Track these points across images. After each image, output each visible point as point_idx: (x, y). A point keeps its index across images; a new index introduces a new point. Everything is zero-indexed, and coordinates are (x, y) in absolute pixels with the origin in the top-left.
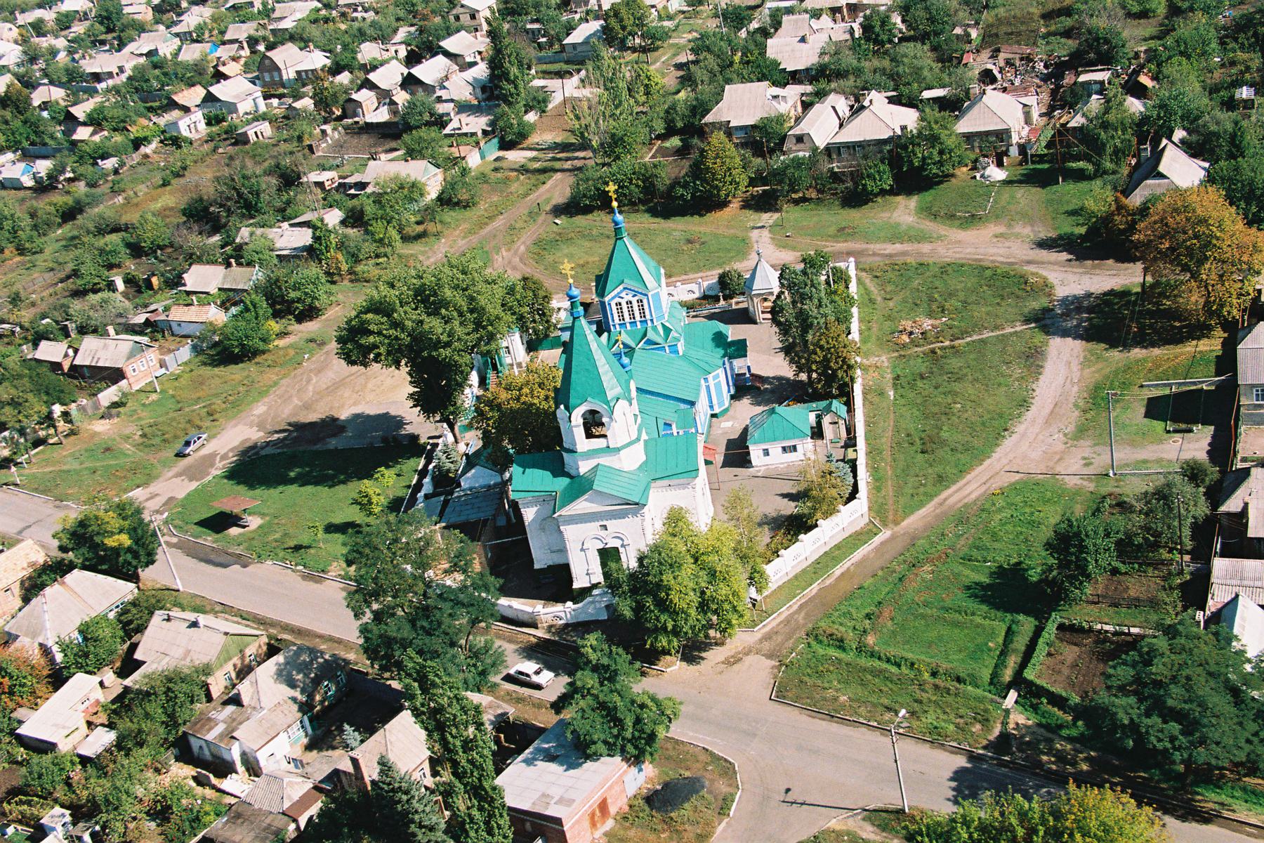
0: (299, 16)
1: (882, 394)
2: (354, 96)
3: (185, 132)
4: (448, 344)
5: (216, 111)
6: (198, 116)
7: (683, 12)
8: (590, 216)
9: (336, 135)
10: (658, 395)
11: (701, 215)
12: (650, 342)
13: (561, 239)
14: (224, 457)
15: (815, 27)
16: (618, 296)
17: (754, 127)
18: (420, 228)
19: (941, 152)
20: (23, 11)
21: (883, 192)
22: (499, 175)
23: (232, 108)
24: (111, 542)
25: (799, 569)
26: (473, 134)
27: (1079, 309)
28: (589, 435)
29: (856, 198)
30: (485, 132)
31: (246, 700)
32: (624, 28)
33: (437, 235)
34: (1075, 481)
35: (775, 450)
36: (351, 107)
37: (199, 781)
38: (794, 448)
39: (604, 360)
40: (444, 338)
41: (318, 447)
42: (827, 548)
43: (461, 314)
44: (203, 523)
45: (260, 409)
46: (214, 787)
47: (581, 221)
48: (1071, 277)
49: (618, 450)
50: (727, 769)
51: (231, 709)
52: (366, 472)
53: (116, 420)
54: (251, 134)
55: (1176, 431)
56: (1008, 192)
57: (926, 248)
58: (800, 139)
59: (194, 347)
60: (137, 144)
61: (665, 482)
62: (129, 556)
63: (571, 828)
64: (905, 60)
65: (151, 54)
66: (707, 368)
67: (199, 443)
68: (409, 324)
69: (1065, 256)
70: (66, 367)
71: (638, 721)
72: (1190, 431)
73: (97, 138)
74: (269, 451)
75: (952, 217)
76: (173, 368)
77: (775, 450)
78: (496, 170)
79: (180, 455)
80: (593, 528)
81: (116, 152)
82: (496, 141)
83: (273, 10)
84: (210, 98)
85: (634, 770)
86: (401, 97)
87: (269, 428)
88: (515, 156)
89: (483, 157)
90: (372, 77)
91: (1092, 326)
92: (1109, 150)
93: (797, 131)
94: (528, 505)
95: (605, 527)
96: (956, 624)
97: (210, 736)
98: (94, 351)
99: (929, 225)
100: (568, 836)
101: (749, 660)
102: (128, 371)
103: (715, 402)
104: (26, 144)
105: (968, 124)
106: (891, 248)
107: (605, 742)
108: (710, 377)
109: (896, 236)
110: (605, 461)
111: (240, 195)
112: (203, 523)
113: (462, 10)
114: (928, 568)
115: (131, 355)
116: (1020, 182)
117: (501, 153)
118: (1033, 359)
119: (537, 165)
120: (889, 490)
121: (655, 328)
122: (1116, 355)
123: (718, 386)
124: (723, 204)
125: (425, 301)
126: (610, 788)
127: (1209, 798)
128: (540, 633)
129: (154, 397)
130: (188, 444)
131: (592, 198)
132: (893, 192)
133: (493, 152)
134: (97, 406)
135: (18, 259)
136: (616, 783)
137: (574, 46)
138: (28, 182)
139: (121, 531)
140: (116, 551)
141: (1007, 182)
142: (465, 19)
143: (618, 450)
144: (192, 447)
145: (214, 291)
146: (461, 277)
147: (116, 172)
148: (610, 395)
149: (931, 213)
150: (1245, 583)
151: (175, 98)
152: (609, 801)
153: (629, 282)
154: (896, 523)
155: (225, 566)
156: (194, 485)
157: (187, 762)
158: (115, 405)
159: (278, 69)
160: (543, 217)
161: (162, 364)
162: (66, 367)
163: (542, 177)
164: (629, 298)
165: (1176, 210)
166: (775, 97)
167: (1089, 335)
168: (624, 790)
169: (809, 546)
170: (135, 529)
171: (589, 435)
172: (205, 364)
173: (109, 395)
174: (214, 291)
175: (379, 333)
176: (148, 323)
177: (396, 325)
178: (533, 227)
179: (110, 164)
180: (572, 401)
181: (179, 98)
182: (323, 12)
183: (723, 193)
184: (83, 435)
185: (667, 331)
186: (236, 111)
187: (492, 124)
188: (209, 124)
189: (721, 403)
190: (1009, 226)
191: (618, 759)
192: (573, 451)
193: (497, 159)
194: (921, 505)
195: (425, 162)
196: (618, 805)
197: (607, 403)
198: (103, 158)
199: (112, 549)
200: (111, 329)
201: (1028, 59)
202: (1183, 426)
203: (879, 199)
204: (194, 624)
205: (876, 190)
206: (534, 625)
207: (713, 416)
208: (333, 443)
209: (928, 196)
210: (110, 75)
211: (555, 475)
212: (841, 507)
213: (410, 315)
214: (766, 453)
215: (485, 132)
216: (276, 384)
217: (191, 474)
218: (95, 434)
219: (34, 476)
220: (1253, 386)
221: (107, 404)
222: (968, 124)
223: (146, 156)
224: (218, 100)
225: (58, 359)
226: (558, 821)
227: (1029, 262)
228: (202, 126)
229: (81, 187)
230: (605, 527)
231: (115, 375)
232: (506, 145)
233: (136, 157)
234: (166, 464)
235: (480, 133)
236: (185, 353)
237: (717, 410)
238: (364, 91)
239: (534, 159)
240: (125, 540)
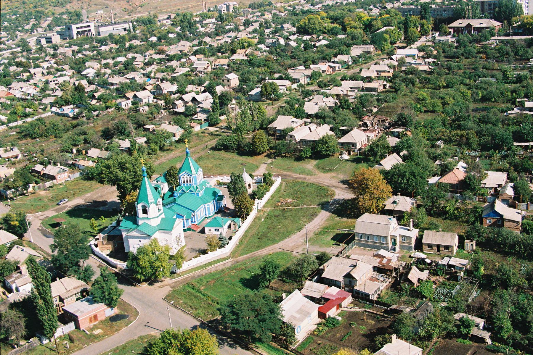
0: (181, 73)
1: (260, 219)
2: (176, 102)
3: (124, 107)
4: (124, 181)
5: (136, 101)
6: (129, 102)
7: (296, 89)
8: (220, 152)
9: (166, 114)
10: (187, 208)
11: (252, 156)
12: (191, 191)
13: (207, 157)
14: (70, 207)
15: (324, 100)
16: (183, 175)
17: (283, 130)
18: (168, 148)
19: (328, 147)
20: (104, 59)
21: (307, 158)
22: (203, 134)
23: (141, 100)
24: (13, 223)
25: (198, 265)
26: (201, 120)
27: (338, 204)
28: (144, 213)
29: (299, 159)
30: (205, 120)
31: (23, 273)
32: (267, 92)
33: (172, 150)
34: (297, 254)
35: (213, 229)
36: (175, 106)
37: (4, 293)
38: (218, 230)
39: (150, 191)
40: (122, 179)
41: (97, 209)
42: (210, 261)
43: (130, 172)
44: (51, 225)
45: (88, 195)
46: (6, 296)
47: (216, 153)
48: (342, 193)
49: (150, 219)
50: (137, 313)
51: (19, 274)
52: (97, 218)
53: (48, 191)
54: (141, 110)
55: (335, 244)
56: (349, 164)
57: (308, 177)
58: (291, 136)
59: (81, 174)
60: (107, 108)
61: (162, 231)
62: (19, 229)
63: (82, 319)
64: (341, 115)
65: (133, 79)
66: (206, 201)
67: (64, 202)
68: (114, 173)
69: (346, 186)
70: (42, 174)
71: (109, 294)
72: (339, 245)
73: (98, 104)
74: (82, 207)
75: (323, 168)
76: (72, 179)
77: (213, 229)
78: (203, 133)
79: (58, 205)
80: (137, 241)
81: (101, 109)
82: (207, 123)
83: (175, 70)
84: (135, 96)
85: (109, 309)
86: (190, 104)
87: (87, 201)
88: (212, 129)
89: (201, 128)
90: (183, 97)
91: (337, 209)
92: (378, 154)
93: (291, 134)
94: (124, 231)
95: (140, 241)
96: (230, 288)
97: (9, 281)
98: (51, 170)
99: (316, 171)
100: (80, 322)
101: (168, 287)
102: (57, 177)
103: (207, 212)
104: (78, 103)
105: (345, 139)
106: (298, 176)
107: (100, 298)
108: (206, 205)
109: (304, 172)
110: (147, 221)
111: (118, 128)
112: (51, 225)
113: (225, 78)
114: (234, 271)
115: (59, 172)
116: (351, 161)
117: (207, 128)
118: (313, 216)
119: (217, 133)
120: (241, 248)
121: (193, 187)
122: (338, 219)
123: (209, 208)
124: (259, 154)
125: (121, 166)
126: (99, 312)
127: (253, 346)
128: (117, 270)
129: (62, 186)
130: (61, 201)
131: (221, 146)
132: (311, 158)
133: (205, 126)
134: (44, 186)
135: (55, 139)
136: (102, 311)
137: (252, 95)
138: (71, 115)
139: (17, 220)
140: (15, 226)
141: (347, 160)
142: (226, 81)
143: (150, 219)
144: (62, 202)
145: (95, 157)
146: (135, 161)
147: (97, 116)
148: (150, 201)
149: (318, 167)
150: (312, 290)
151: (126, 95)
152: (98, 316)
153: (187, 171)
154: (236, 258)
155: (48, 237)
156: (57, 214)
157: (4, 288)
158: (51, 187)
159: (162, 90)
160: (207, 150)
161: (69, 177)
162: (42, 174)
163: (215, 137)
164: (187, 176)
165: (524, 189)
166: (293, 122)
167: (334, 212)
168: (105, 314)
169: (203, 259)
170: (21, 221)
171: (144, 213)
172: (82, 179)
173: (48, 184)
174: (95, 157)
175: (105, 174)
176: (73, 164)
177: (111, 173)
178: (201, 153)
179: (96, 113)
180: (139, 201)
181: (127, 95)
182: (190, 73)
183: (258, 150)
184: (36, 194)
185: (197, 188)
186: (142, 102)
187: (207, 117)
188: (132, 105)
189: (209, 214)
190: (338, 174)
191: (104, 304)
192: (138, 217)
193: (206, 129)
194: (246, 254)
195: (178, 127)
196: (101, 318)
197: (148, 204)
198: (94, 111)
199: (13, 225)
200: (59, 164)
201: (383, 121)
202: (338, 243)
203: (306, 160)
204: (23, 250)
205: (304, 157)
206: (116, 268)
207: (206, 217)
208: (101, 208)
209: (322, 161)
210: (116, 84)
211: (133, 224)
212: (218, 249)
213: (115, 170)
214: (210, 230)
215: (205, 120)
216: (98, 188)
217: (57, 211)
218: (40, 194)
219: (15, 204)
220: (359, 233)
221: (48, 186)
222: (345, 139)
223: (109, 112)
224: (137, 97)
225: (40, 170)
226: (77, 317)
227: (334, 186)
228: (130, 105)
229: (85, 119)
230: (140, 241)
231: (53, 178)
232: (210, 125)
233: (106, 112)
234: (53, 207)
235: (203, 120)
236: (77, 175)
237: (207, 216)
238: (180, 101)
239: (217, 131)
240: (17, 223)
